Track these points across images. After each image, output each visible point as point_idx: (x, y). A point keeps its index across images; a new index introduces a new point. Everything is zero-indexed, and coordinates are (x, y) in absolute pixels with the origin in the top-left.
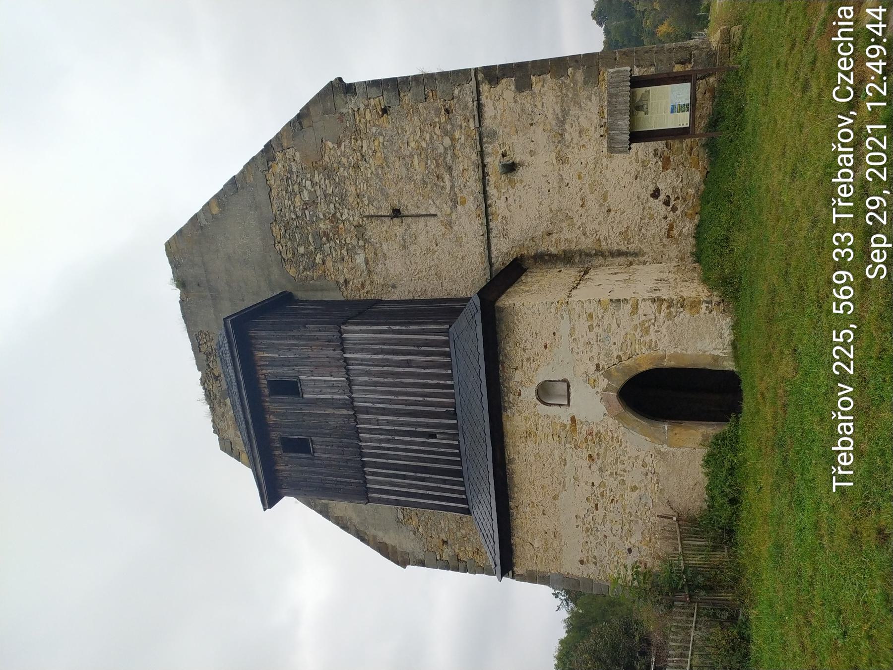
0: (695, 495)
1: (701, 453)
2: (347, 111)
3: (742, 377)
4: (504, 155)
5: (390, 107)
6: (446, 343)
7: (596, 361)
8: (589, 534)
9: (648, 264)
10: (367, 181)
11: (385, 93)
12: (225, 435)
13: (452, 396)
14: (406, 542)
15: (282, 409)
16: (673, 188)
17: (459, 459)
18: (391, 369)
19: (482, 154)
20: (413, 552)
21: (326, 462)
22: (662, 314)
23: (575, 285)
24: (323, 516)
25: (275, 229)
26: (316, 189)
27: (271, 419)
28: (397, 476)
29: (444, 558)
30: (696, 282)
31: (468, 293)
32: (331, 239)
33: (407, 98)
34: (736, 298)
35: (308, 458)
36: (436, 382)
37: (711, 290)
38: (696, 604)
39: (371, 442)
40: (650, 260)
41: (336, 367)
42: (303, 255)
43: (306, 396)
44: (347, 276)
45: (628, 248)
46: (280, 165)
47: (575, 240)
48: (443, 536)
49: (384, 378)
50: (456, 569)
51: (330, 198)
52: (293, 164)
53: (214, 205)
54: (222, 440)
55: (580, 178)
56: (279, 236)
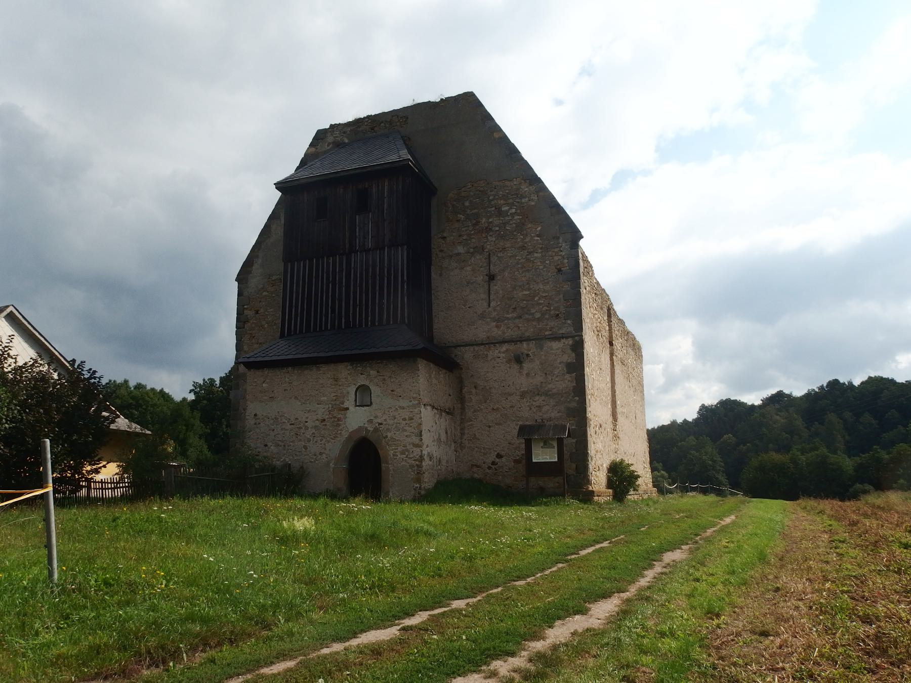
2: (561, 242)
9: (455, 453)
14: (255, 282)
19: (528, 340)
22: (413, 462)
31: (435, 330)
33: (567, 287)
42: (463, 204)
44: (448, 239)
46: (527, 189)
49: (371, 277)
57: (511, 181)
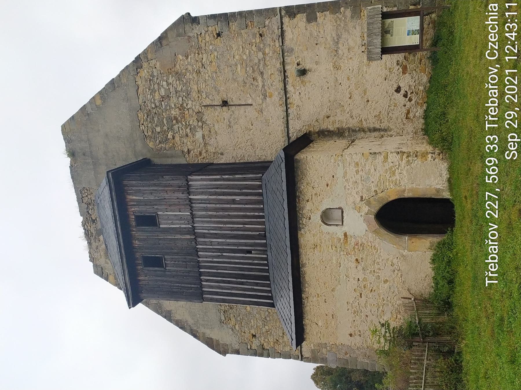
0: (425, 284)
1: (430, 254)
3: (455, 203)
4: (298, 64)
5: (222, 32)
6: (260, 187)
7: (361, 194)
8: (356, 314)
9: (393, 136)
10: (205, 82)
11: (219, 23)
12: (98, 263)
13: (263, 223)
15: (144, 236)
16: (410, 86)
17: (267, 268)
18: (221, 206)
19: (283, 63)
20: (232, 344)
21: (174, 273)
22: (404, 161)
23: (346, 148)
24: (167, 320)
25: (140, 115)
26: (170, 87)
27: (136, 243)
28: (224, 282)
29: (253, 348)
30: (425, 145)
31: (273, 158)
32: (179, 122)
33: (234, 26)
34: (450, 149)
35: (161, 271)
36: (252, 214)
37: (435, 147)
38: (427, 343)
39: (206, 258)
40: (395, 134)
41: (183, 205)
42: (159, 133)
43: (161, 226)
45: (380, 126)
46: (145, 71)
47: (345, 121)
48: (253, 332)
49: (217, 212)
50: (261, 355)
51: (179, 94)
52: (154, 70)
53: (98, 98)
54: (96, 266)
55: (348, 79)
56: (142, 120)
57: (138, 87)
